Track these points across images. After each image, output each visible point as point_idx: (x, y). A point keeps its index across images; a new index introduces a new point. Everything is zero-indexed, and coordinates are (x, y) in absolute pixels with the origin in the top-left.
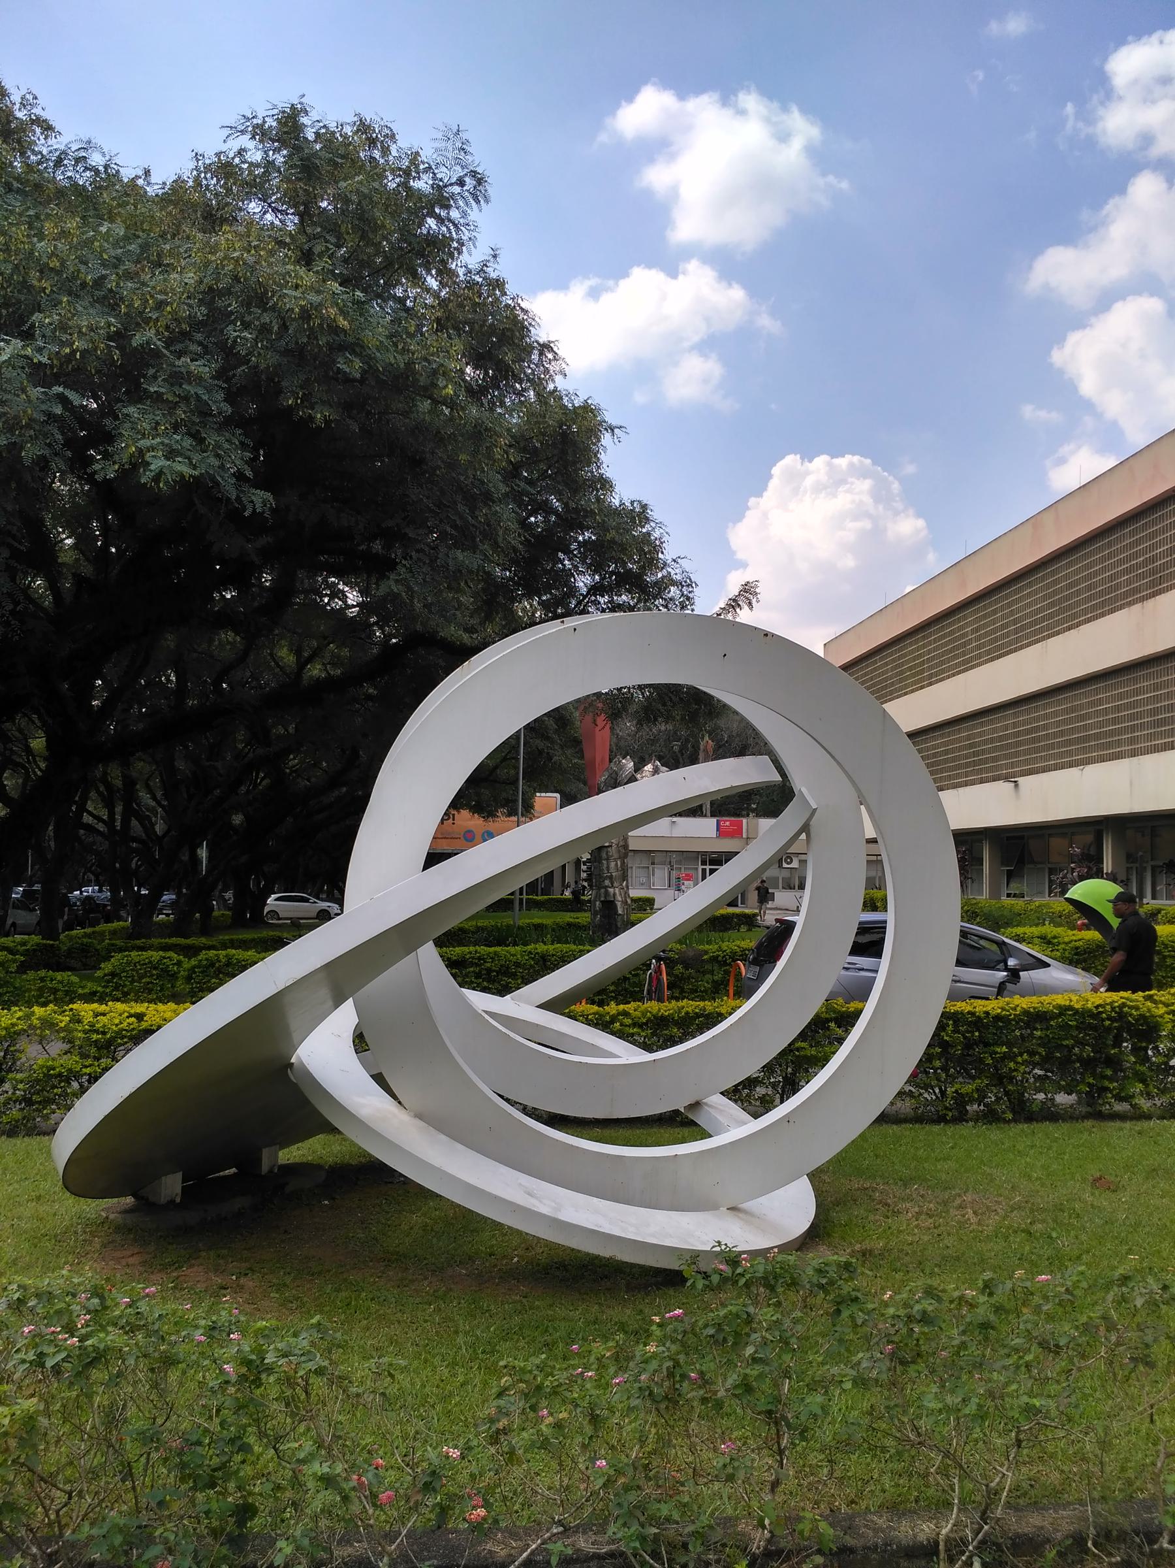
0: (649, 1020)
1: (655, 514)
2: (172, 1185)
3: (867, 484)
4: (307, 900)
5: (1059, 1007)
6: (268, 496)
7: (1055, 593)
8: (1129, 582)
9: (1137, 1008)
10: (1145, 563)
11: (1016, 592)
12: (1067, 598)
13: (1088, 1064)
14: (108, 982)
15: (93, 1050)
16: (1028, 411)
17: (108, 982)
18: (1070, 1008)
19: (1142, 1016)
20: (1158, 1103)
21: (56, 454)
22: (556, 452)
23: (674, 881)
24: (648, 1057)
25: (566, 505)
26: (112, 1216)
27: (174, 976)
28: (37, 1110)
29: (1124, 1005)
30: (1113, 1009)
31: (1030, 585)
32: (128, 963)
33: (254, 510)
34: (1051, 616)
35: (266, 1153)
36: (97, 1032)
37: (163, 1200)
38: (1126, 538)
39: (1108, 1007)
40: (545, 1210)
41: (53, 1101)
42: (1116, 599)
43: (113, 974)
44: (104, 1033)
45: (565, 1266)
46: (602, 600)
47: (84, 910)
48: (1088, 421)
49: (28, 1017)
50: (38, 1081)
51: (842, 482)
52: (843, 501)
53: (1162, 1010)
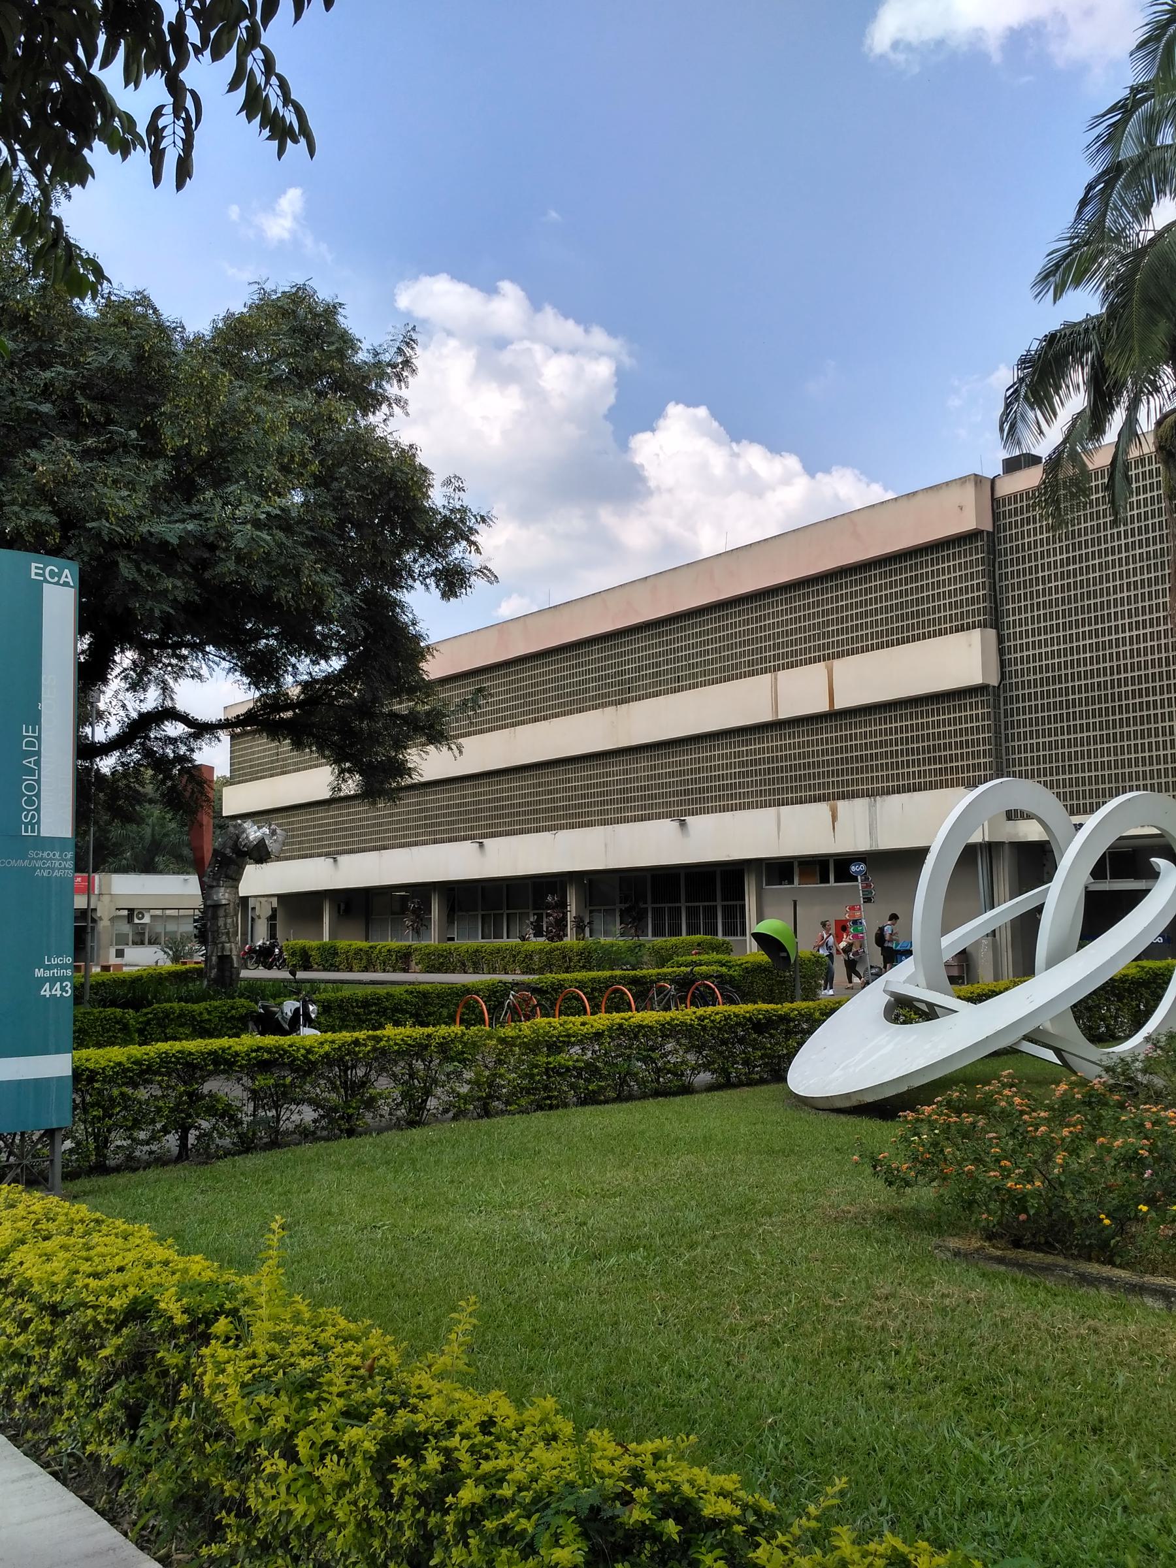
8: (598, 688)
10: (614, 675)
11: (678, 630)
42: (584, 700)
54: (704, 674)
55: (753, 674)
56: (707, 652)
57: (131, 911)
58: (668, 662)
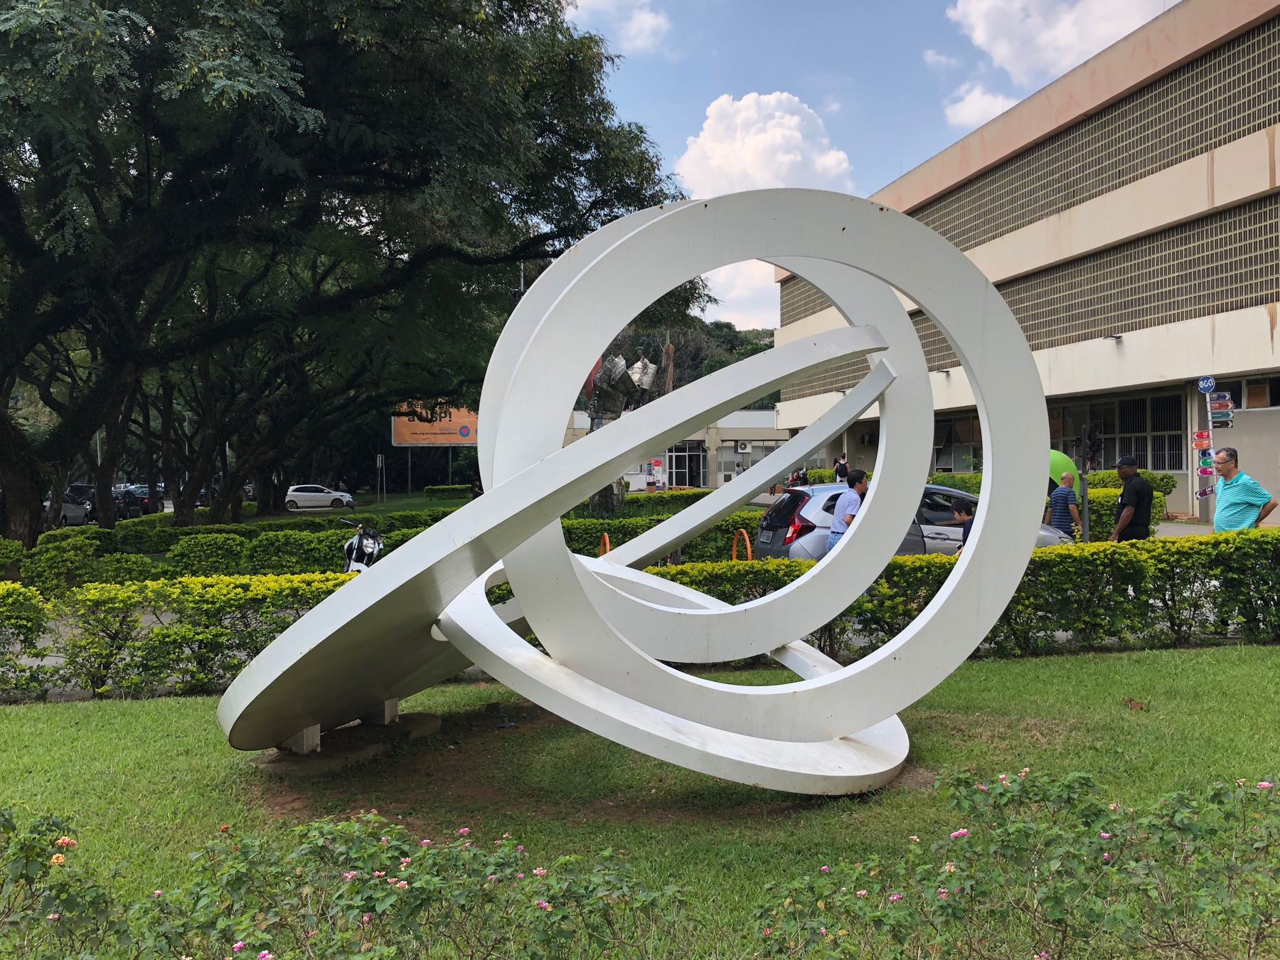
0: (705, 578)
1: (651, 134)
2: (312, 736)
3: (795, 120)
4: (322, 491)
5: (1060, 555)
6: (319, 113)
7: (980, 207)
8: (1046, 196)
9: (1126, 555)
12: (991, 211)
13: (1085, 606)
14: (178, 562)
15: (204, 618)
16: (930, 56)
17: (178, 562)
18: (1069, 556)
19: (1130, 561)
20: (1141, 636)
21: (122, 75)
22: (563, 78)
23: (645, 467)
24: (725, 608)
25: (570, 127)
26: (262, 766)
27: (237, 556)
28: (153, 674)
29: (1114, 552)
30: (1106, 556)
31: (959, 199)
32: (196, 545)
33: (307, 126)
34: (977, 227)
35: (387, 703)
36: (207, 602)
37: (306, 750)
38: (1044, 156)
39: (1102, 555)
40: (695, 745)
41: (167, 666)
43: (182, 555)
44: (213, 603)
45: (701, 795)
46: (602, 213)
47: (125, 503)
48: (982, 66)
49: (141, 591)
50: (154, 648)
51: (771, 117)
52: (775, 134)
53: (1145, 556)
54: (1144, 164)
55: (1193, 155)
56: (1146, 139)
57: (736, 441)
58: (1109, 156)
